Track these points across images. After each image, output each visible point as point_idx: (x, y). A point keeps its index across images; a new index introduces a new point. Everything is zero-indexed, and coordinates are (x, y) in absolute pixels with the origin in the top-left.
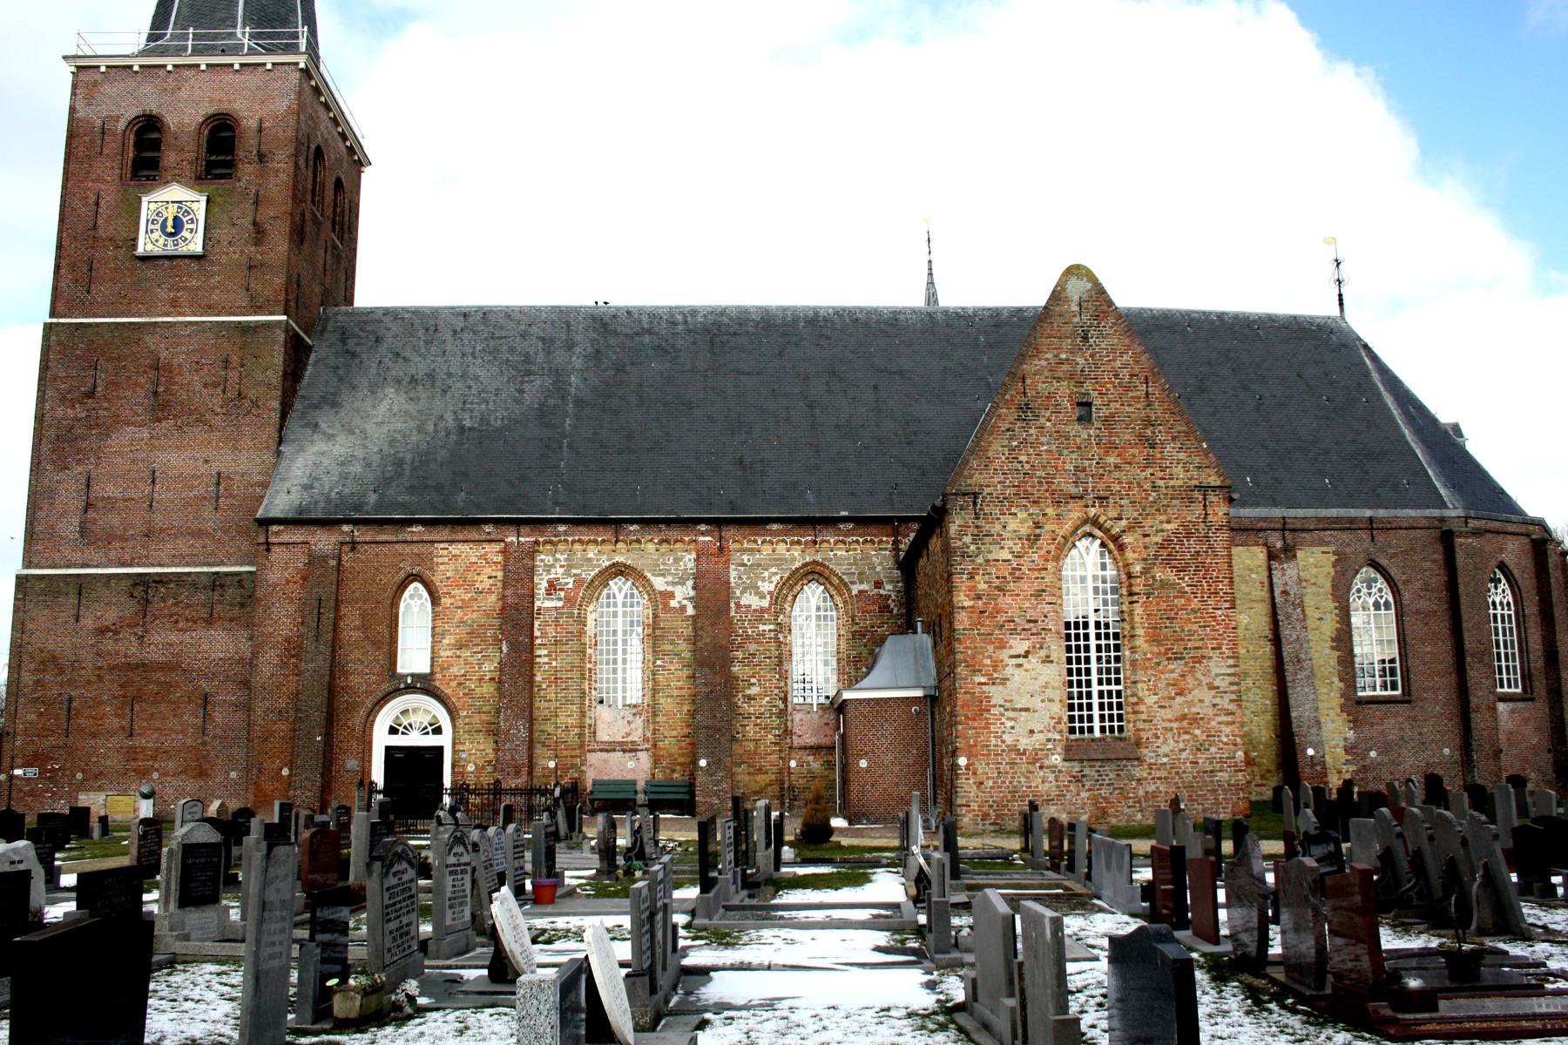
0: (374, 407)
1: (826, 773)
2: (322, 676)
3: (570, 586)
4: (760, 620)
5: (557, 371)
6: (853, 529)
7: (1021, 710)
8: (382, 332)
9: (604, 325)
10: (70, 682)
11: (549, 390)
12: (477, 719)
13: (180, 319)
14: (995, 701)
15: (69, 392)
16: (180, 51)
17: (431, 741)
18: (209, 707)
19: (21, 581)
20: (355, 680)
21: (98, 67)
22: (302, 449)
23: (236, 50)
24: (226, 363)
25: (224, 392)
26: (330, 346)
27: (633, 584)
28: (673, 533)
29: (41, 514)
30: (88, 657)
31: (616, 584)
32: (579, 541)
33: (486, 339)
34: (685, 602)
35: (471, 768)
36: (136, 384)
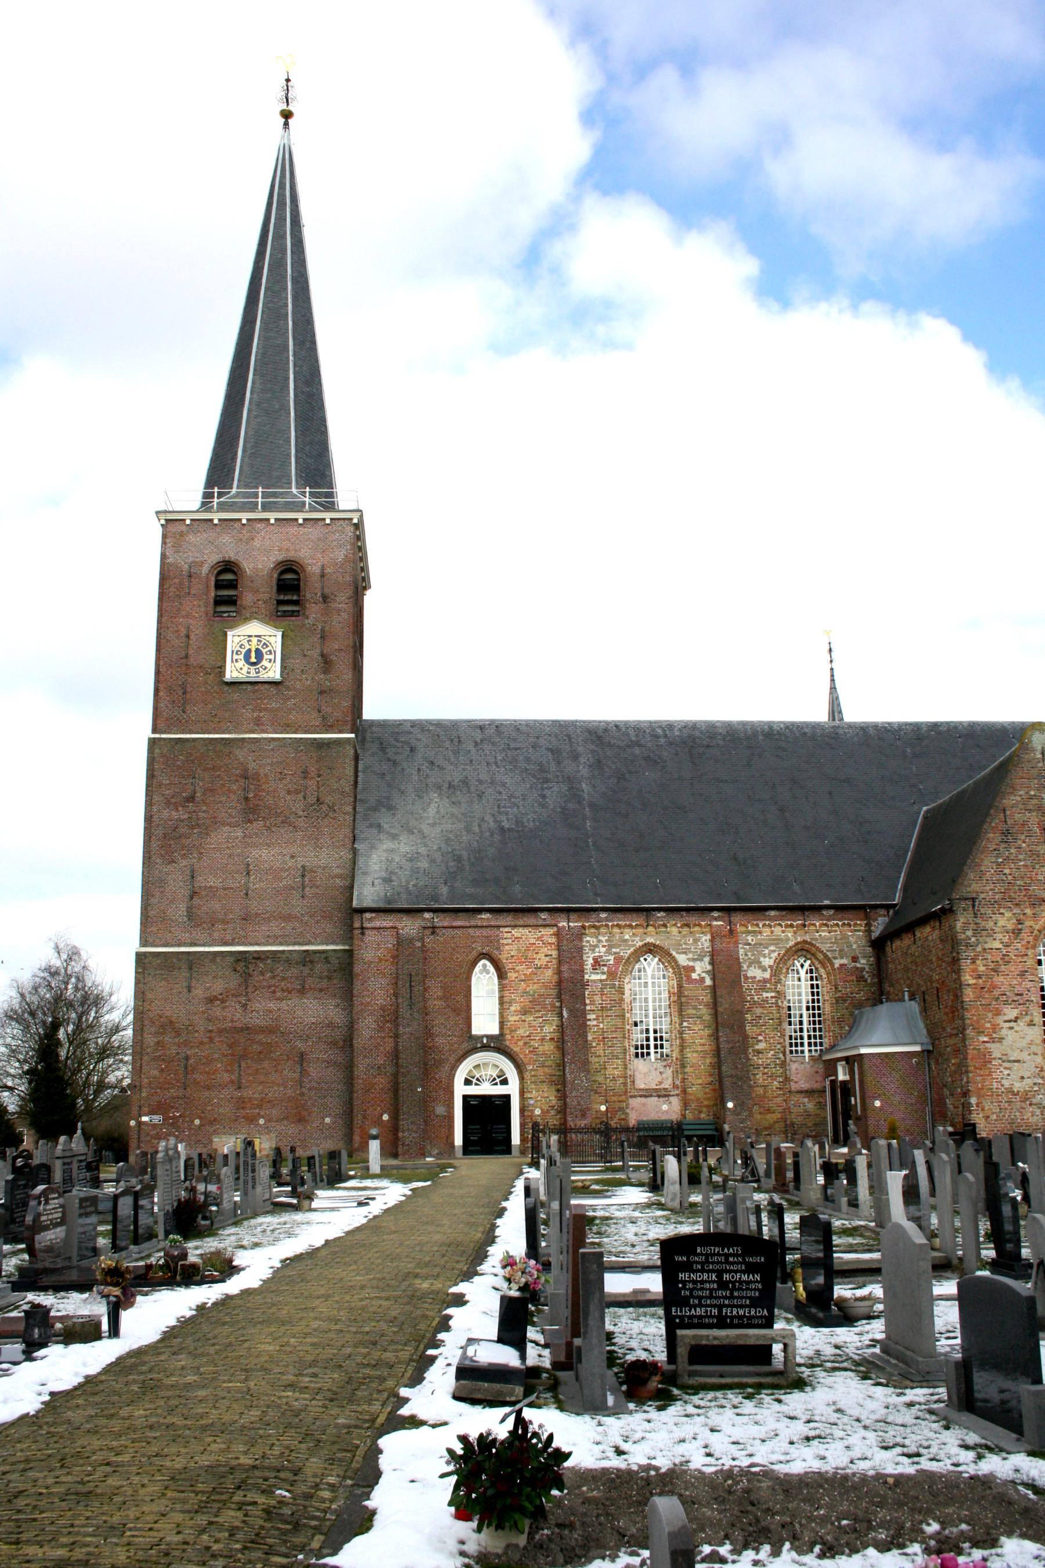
0: (424, 810)
1: (818, 1112)
2: (417, 1039)
3: (612, 962)
4: (764, 989)
5: (568, 778)
6: (834, 914)
7: (1015, 1061)
8: (413, 742)
9: (599, 738)
10: (186, 1043)
11: (566, 796)
12: (540, 1072)
13: (265, 736)
14: (996, 1054)
15: (173, 797)
16: (253, 507)
17: (499, 1090)
18: (305, 1064)
19: (140, 958)
20: (440, 1041)
21: (184, 520)
22: (373, 847)
23: (300, 507)
24: (305, 774)
25: (304, 798)
26: (373, 755)
27: (660, 960)
28: (693, 919)
29: (153, 901)
30: (201, 1025)
31: (645, 960)
32: (618, 926)
33: (504, 750)
34: (704, 975)
35: (538, 1112)
36: (229, 791)
